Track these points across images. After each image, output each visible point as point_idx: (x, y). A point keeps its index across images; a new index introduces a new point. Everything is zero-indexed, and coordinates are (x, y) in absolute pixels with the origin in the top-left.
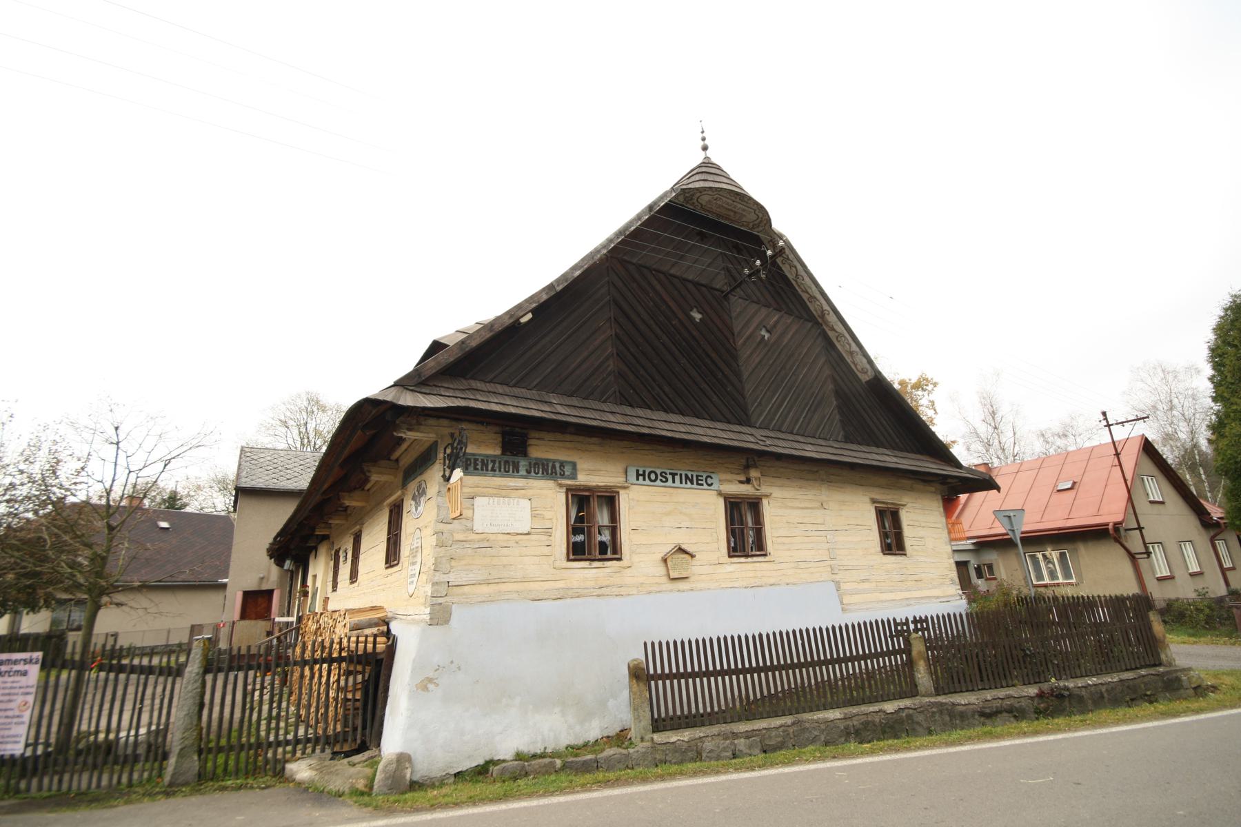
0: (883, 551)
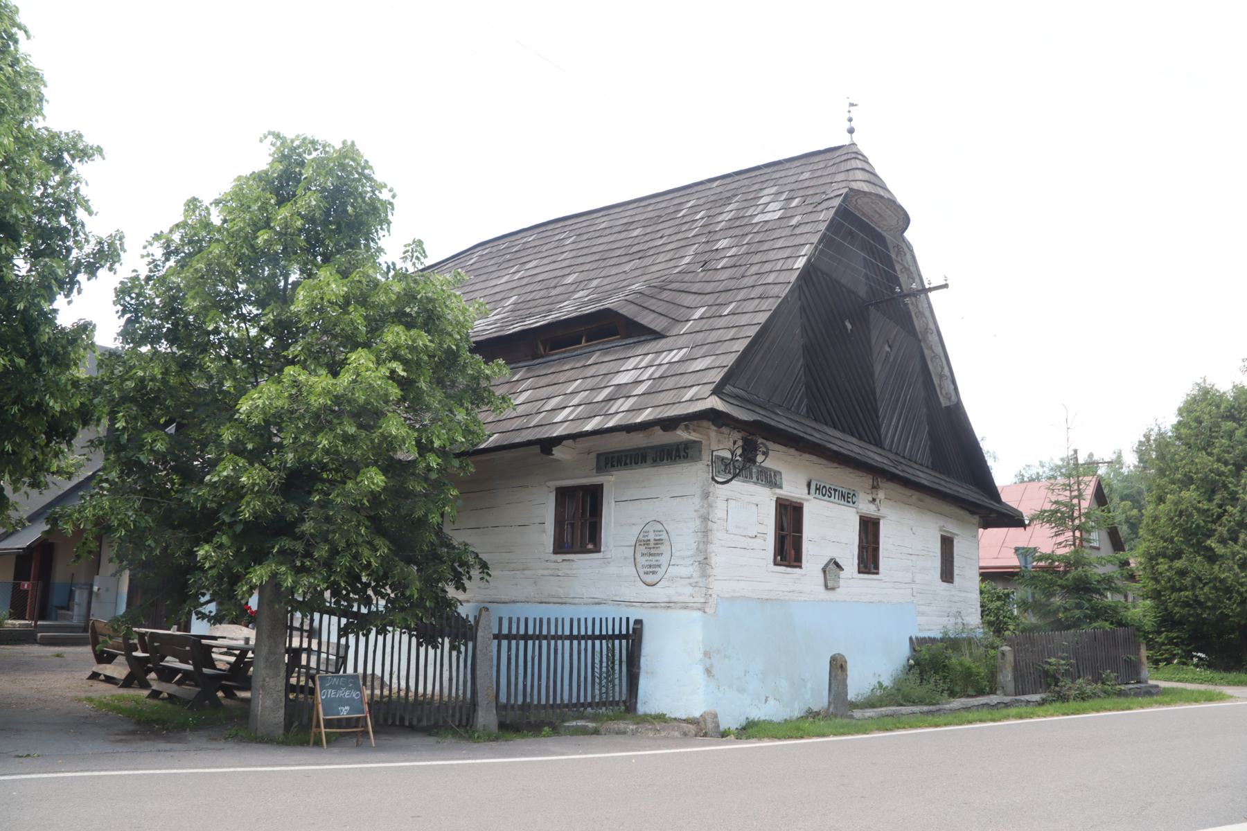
0: (942, 577)
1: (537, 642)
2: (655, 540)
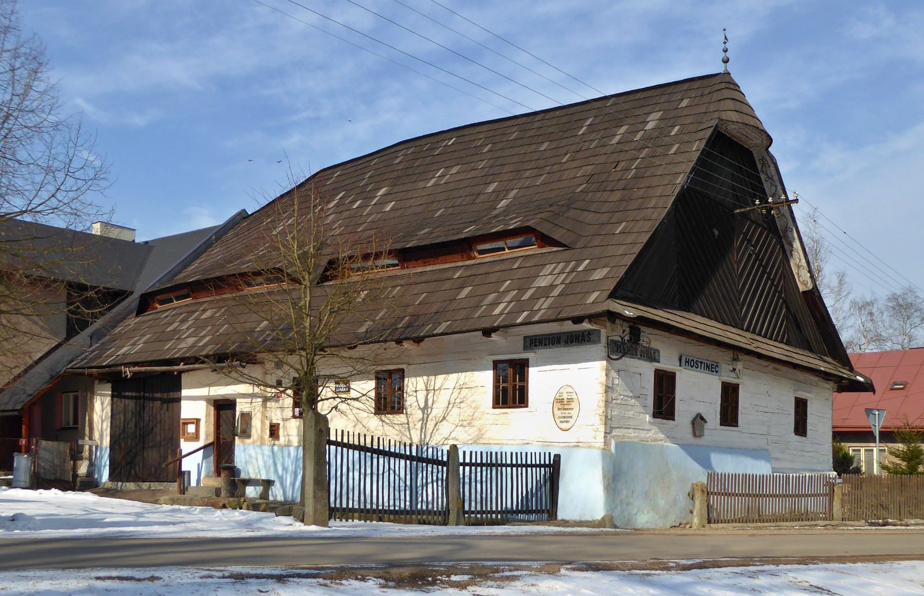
2: (567, 399)
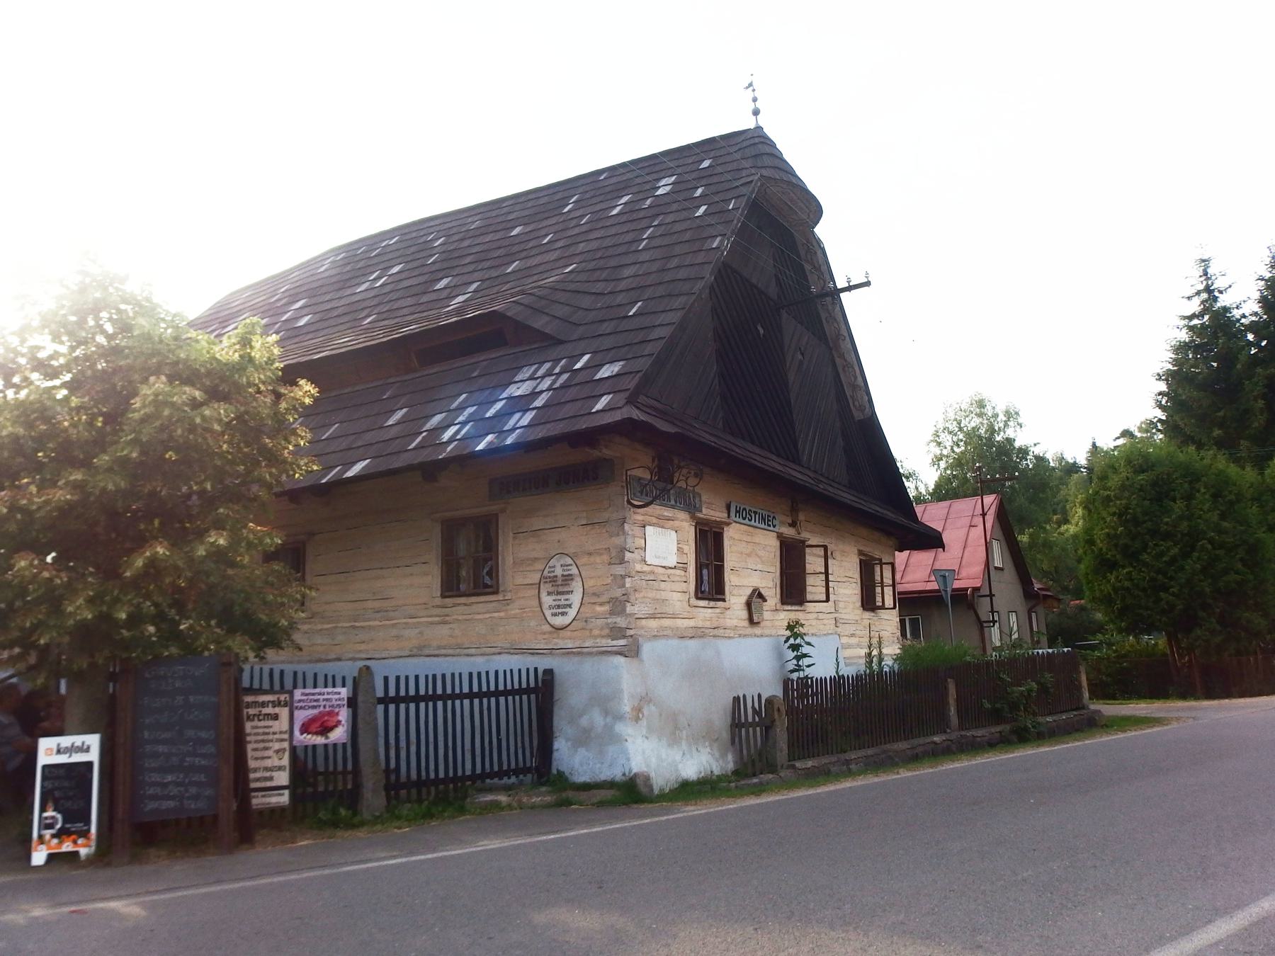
0: (863, 605)
1: (431, 704)
2: (563, 575)
